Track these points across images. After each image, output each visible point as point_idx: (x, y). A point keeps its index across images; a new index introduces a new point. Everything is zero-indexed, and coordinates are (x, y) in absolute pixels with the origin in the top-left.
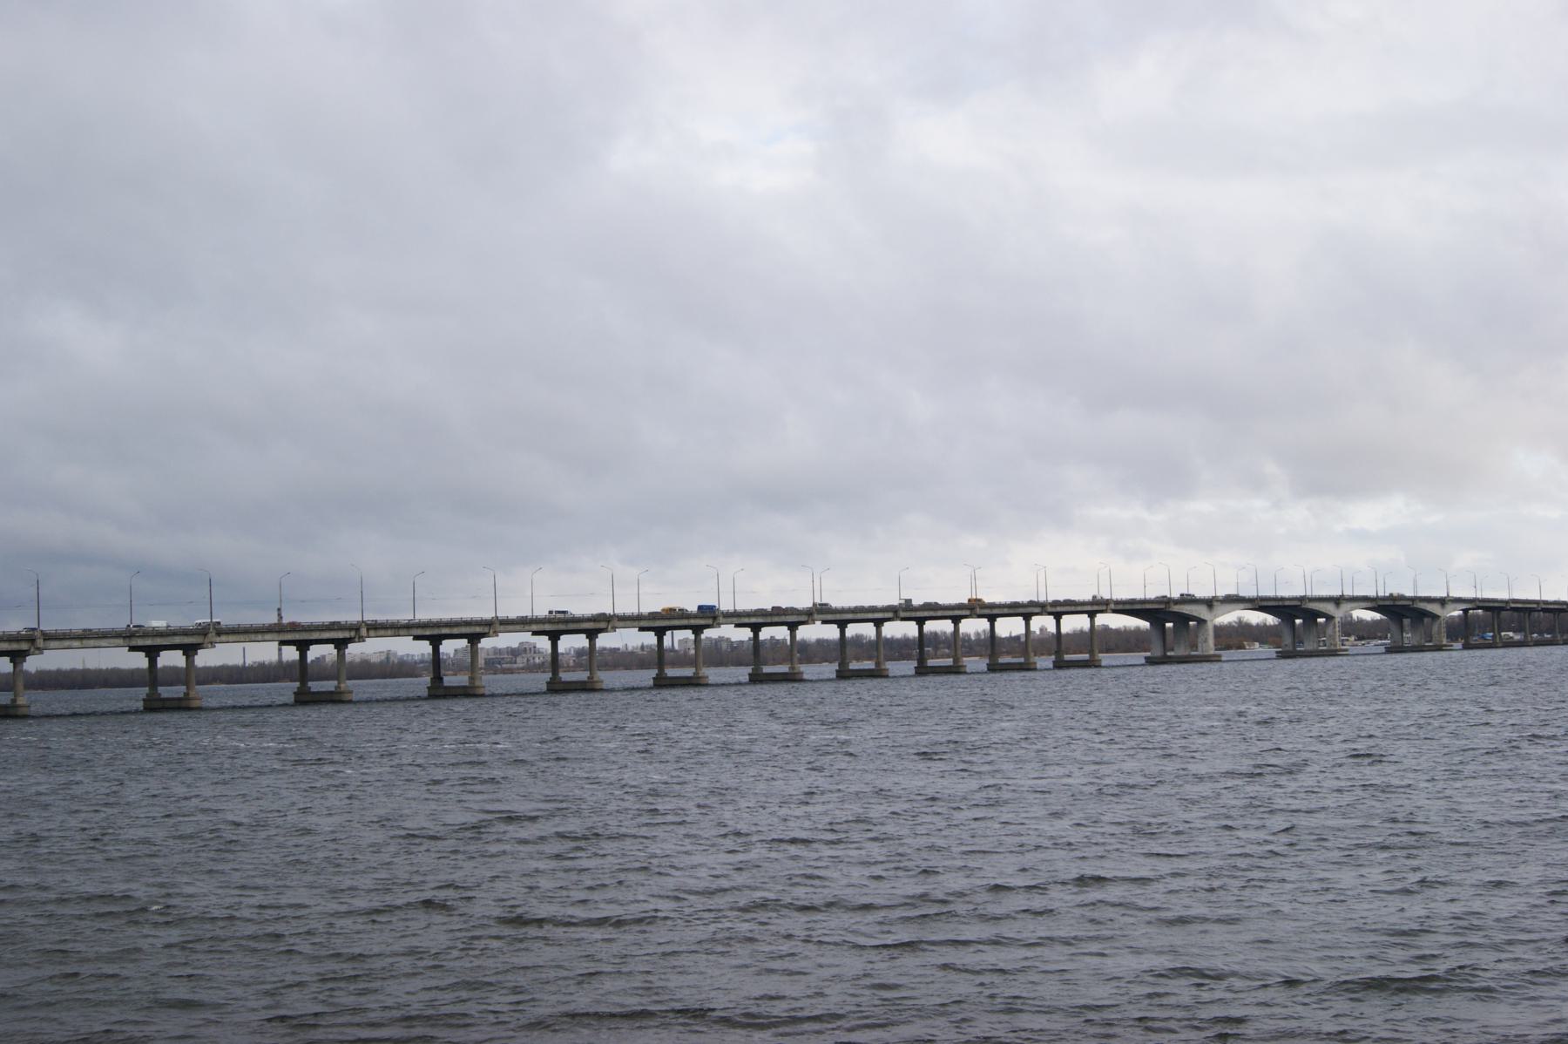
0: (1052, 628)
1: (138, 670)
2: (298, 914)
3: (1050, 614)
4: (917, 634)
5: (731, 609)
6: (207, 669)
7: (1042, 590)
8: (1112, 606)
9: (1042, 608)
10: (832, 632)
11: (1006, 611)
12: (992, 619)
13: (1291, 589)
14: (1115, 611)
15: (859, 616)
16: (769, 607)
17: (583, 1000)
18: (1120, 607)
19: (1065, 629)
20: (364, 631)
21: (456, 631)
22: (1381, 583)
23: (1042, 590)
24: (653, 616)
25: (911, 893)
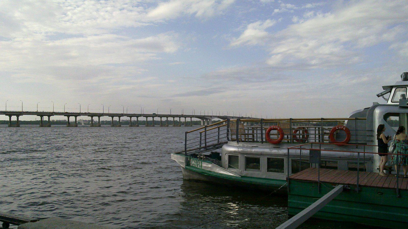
0: (118, 120)
1: (6, 120)
2: (85, 166)
3: (184, 117)
4: (137, 120)
5: (126, 113)
6: (53, 121)
7: (240, 115)
8: (194, 116)
9: (170, 116)
10: (128, 118)
11: (176, 116)
12: (137, 117)
13: (225, 114)
14: (195, 117)
15: (150, 116)
16: (152, 114)
17: (178, 168)
18: (196, 116)
19: (101, 120)
20: (54, 114)
21: (46, 114)
22: (240, 115)
23: (125, 109)
24: (41, 113)
25: (29, 208)
